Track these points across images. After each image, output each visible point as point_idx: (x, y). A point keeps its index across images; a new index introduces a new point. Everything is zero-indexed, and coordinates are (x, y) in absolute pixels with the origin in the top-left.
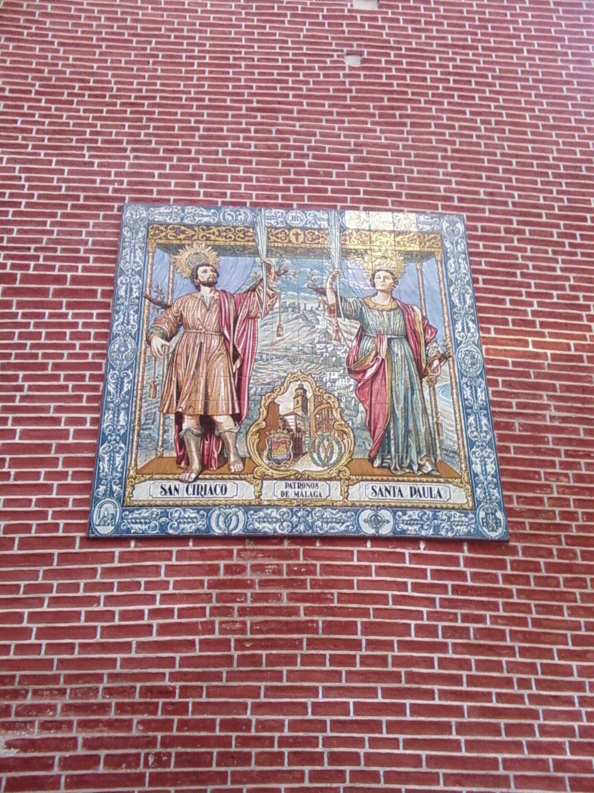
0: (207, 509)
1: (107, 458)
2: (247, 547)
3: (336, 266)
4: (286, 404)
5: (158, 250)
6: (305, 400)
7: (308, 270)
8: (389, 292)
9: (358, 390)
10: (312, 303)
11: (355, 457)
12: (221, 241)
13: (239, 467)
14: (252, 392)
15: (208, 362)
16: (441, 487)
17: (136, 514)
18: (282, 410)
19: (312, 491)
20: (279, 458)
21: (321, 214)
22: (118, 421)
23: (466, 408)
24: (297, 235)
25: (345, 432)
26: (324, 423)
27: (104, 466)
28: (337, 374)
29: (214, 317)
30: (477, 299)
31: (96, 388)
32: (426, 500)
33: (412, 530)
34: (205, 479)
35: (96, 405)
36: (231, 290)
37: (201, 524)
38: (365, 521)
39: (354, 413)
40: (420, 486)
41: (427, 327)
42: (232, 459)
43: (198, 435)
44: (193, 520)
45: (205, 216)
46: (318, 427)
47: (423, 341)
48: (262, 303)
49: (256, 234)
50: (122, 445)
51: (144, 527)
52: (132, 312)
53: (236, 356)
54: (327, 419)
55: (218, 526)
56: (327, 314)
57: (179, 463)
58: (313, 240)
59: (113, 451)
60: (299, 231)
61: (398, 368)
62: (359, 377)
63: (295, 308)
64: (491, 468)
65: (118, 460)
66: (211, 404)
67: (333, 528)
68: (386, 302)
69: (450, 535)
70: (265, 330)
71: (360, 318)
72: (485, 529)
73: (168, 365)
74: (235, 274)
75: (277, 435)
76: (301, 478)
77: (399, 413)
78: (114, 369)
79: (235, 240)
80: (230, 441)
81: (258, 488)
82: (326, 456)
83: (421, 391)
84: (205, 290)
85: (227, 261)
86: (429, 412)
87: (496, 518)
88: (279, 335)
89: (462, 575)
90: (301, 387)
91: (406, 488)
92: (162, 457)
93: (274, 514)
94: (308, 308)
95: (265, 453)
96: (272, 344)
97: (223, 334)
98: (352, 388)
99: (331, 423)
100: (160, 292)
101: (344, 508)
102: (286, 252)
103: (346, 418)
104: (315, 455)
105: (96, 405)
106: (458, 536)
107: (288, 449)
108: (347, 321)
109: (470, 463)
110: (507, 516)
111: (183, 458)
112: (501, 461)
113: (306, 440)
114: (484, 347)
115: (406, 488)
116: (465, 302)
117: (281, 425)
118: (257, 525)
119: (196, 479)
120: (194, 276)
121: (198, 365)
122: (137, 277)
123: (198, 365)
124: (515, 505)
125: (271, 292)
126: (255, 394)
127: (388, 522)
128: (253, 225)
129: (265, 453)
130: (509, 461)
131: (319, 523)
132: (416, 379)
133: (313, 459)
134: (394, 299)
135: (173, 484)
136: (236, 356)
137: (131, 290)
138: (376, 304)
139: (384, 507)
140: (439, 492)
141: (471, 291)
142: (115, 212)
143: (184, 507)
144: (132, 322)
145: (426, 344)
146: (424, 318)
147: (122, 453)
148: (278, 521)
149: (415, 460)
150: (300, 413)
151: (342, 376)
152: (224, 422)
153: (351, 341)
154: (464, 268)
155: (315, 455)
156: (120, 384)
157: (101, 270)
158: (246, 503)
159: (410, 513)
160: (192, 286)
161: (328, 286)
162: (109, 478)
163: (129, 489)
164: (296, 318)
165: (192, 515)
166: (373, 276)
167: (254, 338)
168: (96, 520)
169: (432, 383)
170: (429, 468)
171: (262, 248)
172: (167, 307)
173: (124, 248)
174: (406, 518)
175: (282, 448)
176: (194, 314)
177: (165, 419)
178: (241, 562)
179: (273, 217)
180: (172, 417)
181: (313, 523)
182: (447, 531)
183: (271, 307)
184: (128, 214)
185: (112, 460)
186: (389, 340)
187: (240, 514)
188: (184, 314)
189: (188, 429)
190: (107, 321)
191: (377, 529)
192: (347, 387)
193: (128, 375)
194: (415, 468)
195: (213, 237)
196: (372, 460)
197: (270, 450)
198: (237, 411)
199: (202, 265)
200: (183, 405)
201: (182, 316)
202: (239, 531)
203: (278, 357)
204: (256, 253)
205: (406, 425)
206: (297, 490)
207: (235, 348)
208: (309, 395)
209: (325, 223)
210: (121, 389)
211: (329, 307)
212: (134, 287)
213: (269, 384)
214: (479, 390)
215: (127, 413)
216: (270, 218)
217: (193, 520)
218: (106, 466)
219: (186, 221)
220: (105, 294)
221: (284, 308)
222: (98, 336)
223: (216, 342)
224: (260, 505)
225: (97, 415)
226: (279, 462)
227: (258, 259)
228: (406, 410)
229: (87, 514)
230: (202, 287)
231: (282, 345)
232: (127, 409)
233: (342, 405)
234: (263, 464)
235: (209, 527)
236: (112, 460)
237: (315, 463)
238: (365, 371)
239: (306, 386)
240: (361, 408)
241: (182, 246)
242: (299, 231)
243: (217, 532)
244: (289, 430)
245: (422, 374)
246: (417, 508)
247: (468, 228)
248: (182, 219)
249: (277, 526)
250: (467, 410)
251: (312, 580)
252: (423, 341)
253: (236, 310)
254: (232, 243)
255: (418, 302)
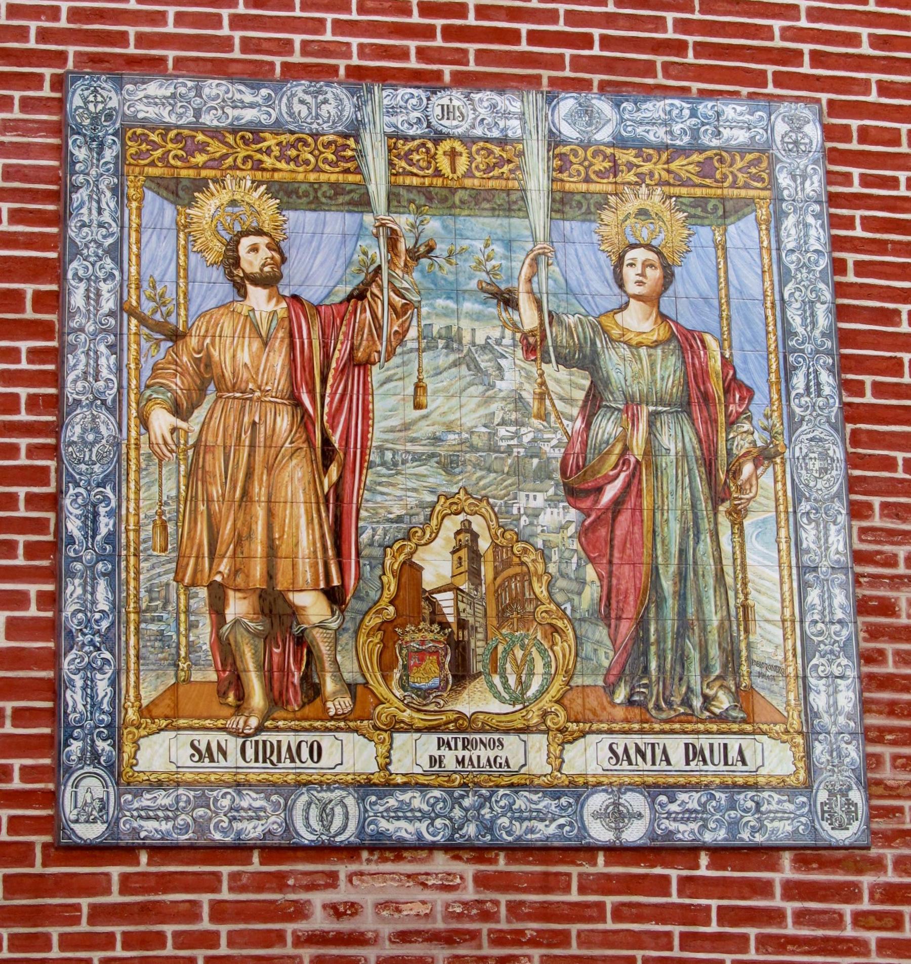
0: (287, 789)
1: (79, 683)
2: (365, 867)
3: (540, 235)
4: (437, 565)
5: (149, 195)
6: (475, 556)
7: (480, 245)
8: (652, 300)
9: (585, 533)
10: (482, 327)
11: (578, 681)
12: (285, 171)
13: (343, 703)
14: (365, 538)
15: (270, 469)
16: (746, 742)
17: (146, 800)
18: (429, 580)
19: (492, 754)
20: (424, 685)
21: (510, 103)
22: (94, 602)
23: (803, 569)
24: (453, 155)
25: (555, 629)
26: (512, 607)
27: (74, 698)
28: (540, 497)
29: (278, 360)
30: (842, 313)
31: (39, 526)
32: (713, 770)
33: (685, 832)
34: (277, 729)
35: (45, 563)
36: (312, 294)
37: (274, 822)
38: (596, 815)
39: (574, 586)
40: (703, 742)
41: (732, 385)
42: (330, 686)
43: (256, 635)
44: (257, 814)
45: (247, 105)
46: (502, 616)
47: (722, 418)
48: (379, 329)
49: (361, 154)
50: (107, 655)
51: (165, 826)
52: (102, 348)
53: (328, 454)
54: (519, 600)
55: (308, 825)
56: (520, 353)
57: (223, 694)
58: (489, 168)
59: (90, 666)
60: (458, 147)
61: (669, 485)
62: (587, 504)
63: (452, 340)
64: (847, 698)
65: (102, 687)
66: (283, 566)
67: (532, 831)
68: (647, 326)
69: (759, 839)
70: (385, 395)
71: (585, 359)
72: (825, 825)
73: (188, 475)
74: (323, 253)
75: (418, 636)
76: (465, 726)
77: (667, 585)
78: (77, 485)
79: (317, 169)
80: (324, 648)
81: (383, 750)
82: (520, 682)
83: (715, 535)
84: (257, 296)
85: (301, 220)
86: (729, 580)
87: (849, 803)
88: (418, 406)
89: (775, 916)
90: (466, 528)
91: (676, 746)
92: (187, 681)
93: (416, 803)
94: (480, 340)
95: (397, 674)
96: (406, 427)
97: (297, 403)
98: (572, 529)
99: (530, 608)
100: (160, 301)
101: (553, 790)
102: (430, 199)
103: (559, 597)
104: (496, 679)
105: (45, 563)
106: (774, 842)
107: (441, 665)
108: (563, 373)
109: (806, 689)
110: (870, 797)
111: (234, 683)
112: (870, 682)
113: (477, 645)
114: (850, 427)
115: (676, 746)
116: (814, 324)
117: (427, 612)
118: (384, 825)
119: (260, 729)
120: (231, 261)
121: (249, 475)
122: (108, 263)
123: (249, 475)
124: (887, 774)
125: (398, 301)
126: (371, 545)
127: (640, 816)
128: (354, 131)
129: (397, 674)
130: (886, 682)
131: (504, 821)
132: (703, 505)
133: (492, 686)
134: (663, 317)
135: (215, 738)
136: (328, 454)
137: (98, 294)
138: (625, 331)
139: (633, 787)
140: (741, 752)
141: (827, 295)
142: (46, 92)
143: (239, 786)
144: (105, 373)
145: (731, 424)
146: (727, 363)
147: (109, 671)
148: (424, 816)
149: (697, 688)
150: (464, 587)
151: (552, 502)
152: (312, 606)
153: (573, 419)
154: (818, 236)
155: (496, 679)
156: (91, 519)
157: (30, 242)
158: (362, 779)
159: (682, 797)
160: (228, 287)
161: (523, 287)
162: (88, 724)
163: (128, 749)
164: (455, 364)
165: (257, 804)
166: (621, 258)
167: (366, 411)
168: (69, 811)
169: (737, 515)
170: (724, 702)
171: (378, 189)
172: (176, 336)
173: (76, 188)
174: (674, 807)
175: (430, 663)
176: (238, 355)
177: (188, 598)
178: (353, 898)
179: (399, 108)
180: (203, 593)
181: (493, 821)
182: (754, 830)
183: (401, 335)
184: (77, 101)
185: (89, 686)
186: (653, 418)
187: (350, 801)
188: (215, 354)
189: (237, 622)
190: (51, 441)
191: (618, 830)
192: (563, 528)
193: (106, 499)
194: (697, 703)
195: (268, 162)
196: (610, 689)
197: (405, 667)
198: (336, 582)
199: (246, 233)
200: (224, 566)
201: (209, 356)
202: (349, 836)
203: (418, 458)
204: (363, 203)
205: (682, 613)
206: (460, 753)
207: (326, 441)
208: (484, 544)
209: (515, 123)
210: (95, 531)
211: (525, 336)
212: (104, 287)
213: (399, 519)
214: (833, 529)
215: (111, 586)
216: (392, 111)
217: (257, 814)
218: (78, 697)
219: (208, 119)
220: (42, 301)
221: (428, 342)
222: (33, 403)
223: (284, 422)
224: (387, 784)
225: (50, 587)
226: (424, 694)
227: (368, 219)
228: (681, 577)
229: (52, 798)
230: (250, 288)
231: (424, 430)
232: (110, 575)
233: (552, 568)
234: (392, 696)
235: (288, 826)
236: (89, 686)
237: (497, 695)
238: (599, 490)
239: (478, 524)
240: (590, 573)
241: (200, 185)
242: (458, 147)
243: (307, 838)
244: (444, 625)
245: (718, 496)
246: (696, 787)
247: (829, 133)
248: (198, 113)
249: (423, 826)
250: (805, 572)
251: (490, 931)
252: (722, 418)
253: (325, 346)
254: (312, 177)
255: (714, 325)
